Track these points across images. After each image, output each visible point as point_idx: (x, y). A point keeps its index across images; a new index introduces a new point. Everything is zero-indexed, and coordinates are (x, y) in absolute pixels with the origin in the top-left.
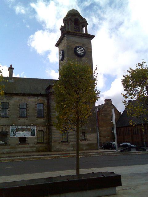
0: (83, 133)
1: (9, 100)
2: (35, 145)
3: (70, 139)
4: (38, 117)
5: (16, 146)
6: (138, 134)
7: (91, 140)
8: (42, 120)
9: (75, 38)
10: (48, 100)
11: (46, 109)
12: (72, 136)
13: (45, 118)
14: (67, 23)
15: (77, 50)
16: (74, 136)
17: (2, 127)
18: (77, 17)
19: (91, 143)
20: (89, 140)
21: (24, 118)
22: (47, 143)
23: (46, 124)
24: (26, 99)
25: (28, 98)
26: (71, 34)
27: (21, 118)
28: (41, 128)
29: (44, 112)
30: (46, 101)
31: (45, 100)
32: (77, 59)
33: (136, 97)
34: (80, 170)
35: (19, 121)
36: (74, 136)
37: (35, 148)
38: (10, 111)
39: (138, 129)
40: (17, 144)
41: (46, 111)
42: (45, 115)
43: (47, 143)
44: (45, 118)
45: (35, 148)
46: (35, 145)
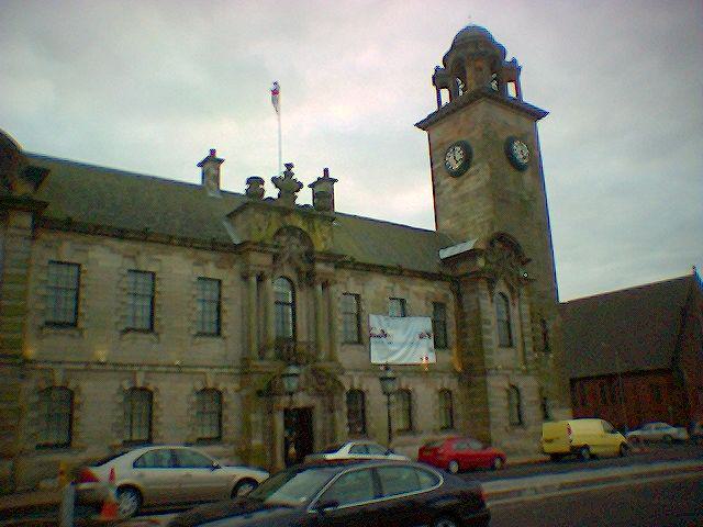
10: (459, 296)
17: (204, 373)
18: (498, 51)
24: (407, 286)
32: (512, 173)
44: (454, 351)
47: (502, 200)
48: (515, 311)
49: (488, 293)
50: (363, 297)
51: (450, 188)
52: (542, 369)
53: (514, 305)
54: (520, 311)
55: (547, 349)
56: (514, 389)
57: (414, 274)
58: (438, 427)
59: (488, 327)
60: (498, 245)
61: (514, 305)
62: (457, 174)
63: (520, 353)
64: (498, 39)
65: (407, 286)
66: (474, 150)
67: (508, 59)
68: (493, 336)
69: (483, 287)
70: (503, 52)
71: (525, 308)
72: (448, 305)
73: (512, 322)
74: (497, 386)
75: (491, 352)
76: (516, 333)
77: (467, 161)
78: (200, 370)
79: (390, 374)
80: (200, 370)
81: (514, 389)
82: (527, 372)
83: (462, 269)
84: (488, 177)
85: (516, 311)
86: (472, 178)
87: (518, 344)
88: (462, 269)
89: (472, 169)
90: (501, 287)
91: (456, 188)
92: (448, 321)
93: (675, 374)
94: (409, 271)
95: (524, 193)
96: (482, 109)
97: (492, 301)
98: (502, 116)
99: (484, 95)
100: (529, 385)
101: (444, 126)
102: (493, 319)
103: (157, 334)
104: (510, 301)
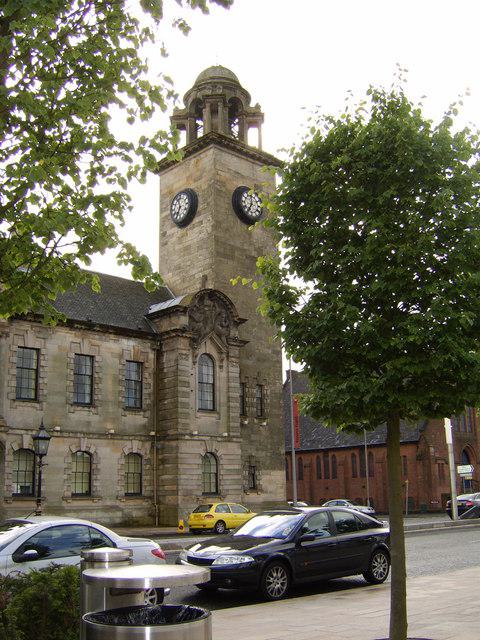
0: (250, 467)
1: (43, 341)
2: (118, 503)
3: (226, 487)
4: (128, 409)
5: (64, 504)
6: (335, 477)
7: (271, 492)
8: (139, 419)
9: (235, 159)
10: (159, 354)
11: (150, 381)
12: (230, 477)
13: (148, 414)
14: (212, 105)
15: (244, 199)
16: (236, 477)
17: (22, 435)
18: (238, 95)
19: (270, 500)
20: (266, 492)
21: (86, 409)
22: (151, 498)
23: (153, 433)
24: (98, 342)
25: (100, 339)
26: (227, 146)
27: (80, 408)
28: (135, 446)
29: (144, 391)
30: (152, 356)
31: (149, 351)
32: (239, 226)
33: (35, 199)
34: (406, 540)
35: (72, 415)
36: (236, 477)
37: (119, 514)
38: (46, 381)
39: (334, 462)
40: (64, 499)
41: (151, 390)
42: (148, 402)
43: (151, 498)
44: (148, 414)
45: (119, 514)
46: (118, 503)
47: (225, 256)
48: (222, 375)
49: (190, 353)
50: (43, 351)
51: (174, 239)
52: (253, 437)
53: (221, 367)
54: (227, 375)
55: (262, 416)
56: (211, 457)
57: (106, 330)
58: (123, 493)
59: (185, 389)
60: (207, 302)
61: (221, 367)
62: (184, 223)
63: (223, 419)
64: (209, 66)
65: (98, 342)
66: (200, 199)
67: (252, 104)
68: (192, 400)
69: (182, 344)
70: (247, 96)
71: (235, 371)
72: (146, 365)
73: (217, 384)
74: (190, 452)
75: (187, 415)
76: (221, 398)
77: (192, 212)
78: (18, 432)
79: (43, 434)
80: (18, 432)
81: (211, 457)
82: (229, 439)
83: (165, 325)
84: (210, 230)
85: (223, 374)
86: (196, 230)
87: (223, 410)
88: (165, 325)
89: (196, 220)
90: (207, 347)
91: (180, 239)
92: (144, 381)
93: (421, 447)
94: (101, 326)
95: (252, 248)
96: (209, 155)
97: (194, 363)
98: (233, 162)
99: (213, 141)
100: (231, 454)
101: (175, 170)
102: (193, 381)
103: (218, 413)
104: (217, 364)
